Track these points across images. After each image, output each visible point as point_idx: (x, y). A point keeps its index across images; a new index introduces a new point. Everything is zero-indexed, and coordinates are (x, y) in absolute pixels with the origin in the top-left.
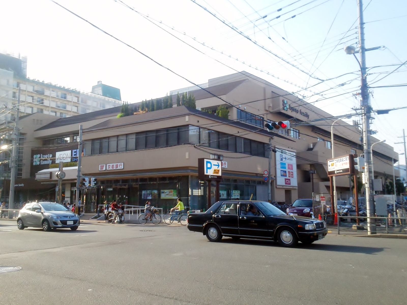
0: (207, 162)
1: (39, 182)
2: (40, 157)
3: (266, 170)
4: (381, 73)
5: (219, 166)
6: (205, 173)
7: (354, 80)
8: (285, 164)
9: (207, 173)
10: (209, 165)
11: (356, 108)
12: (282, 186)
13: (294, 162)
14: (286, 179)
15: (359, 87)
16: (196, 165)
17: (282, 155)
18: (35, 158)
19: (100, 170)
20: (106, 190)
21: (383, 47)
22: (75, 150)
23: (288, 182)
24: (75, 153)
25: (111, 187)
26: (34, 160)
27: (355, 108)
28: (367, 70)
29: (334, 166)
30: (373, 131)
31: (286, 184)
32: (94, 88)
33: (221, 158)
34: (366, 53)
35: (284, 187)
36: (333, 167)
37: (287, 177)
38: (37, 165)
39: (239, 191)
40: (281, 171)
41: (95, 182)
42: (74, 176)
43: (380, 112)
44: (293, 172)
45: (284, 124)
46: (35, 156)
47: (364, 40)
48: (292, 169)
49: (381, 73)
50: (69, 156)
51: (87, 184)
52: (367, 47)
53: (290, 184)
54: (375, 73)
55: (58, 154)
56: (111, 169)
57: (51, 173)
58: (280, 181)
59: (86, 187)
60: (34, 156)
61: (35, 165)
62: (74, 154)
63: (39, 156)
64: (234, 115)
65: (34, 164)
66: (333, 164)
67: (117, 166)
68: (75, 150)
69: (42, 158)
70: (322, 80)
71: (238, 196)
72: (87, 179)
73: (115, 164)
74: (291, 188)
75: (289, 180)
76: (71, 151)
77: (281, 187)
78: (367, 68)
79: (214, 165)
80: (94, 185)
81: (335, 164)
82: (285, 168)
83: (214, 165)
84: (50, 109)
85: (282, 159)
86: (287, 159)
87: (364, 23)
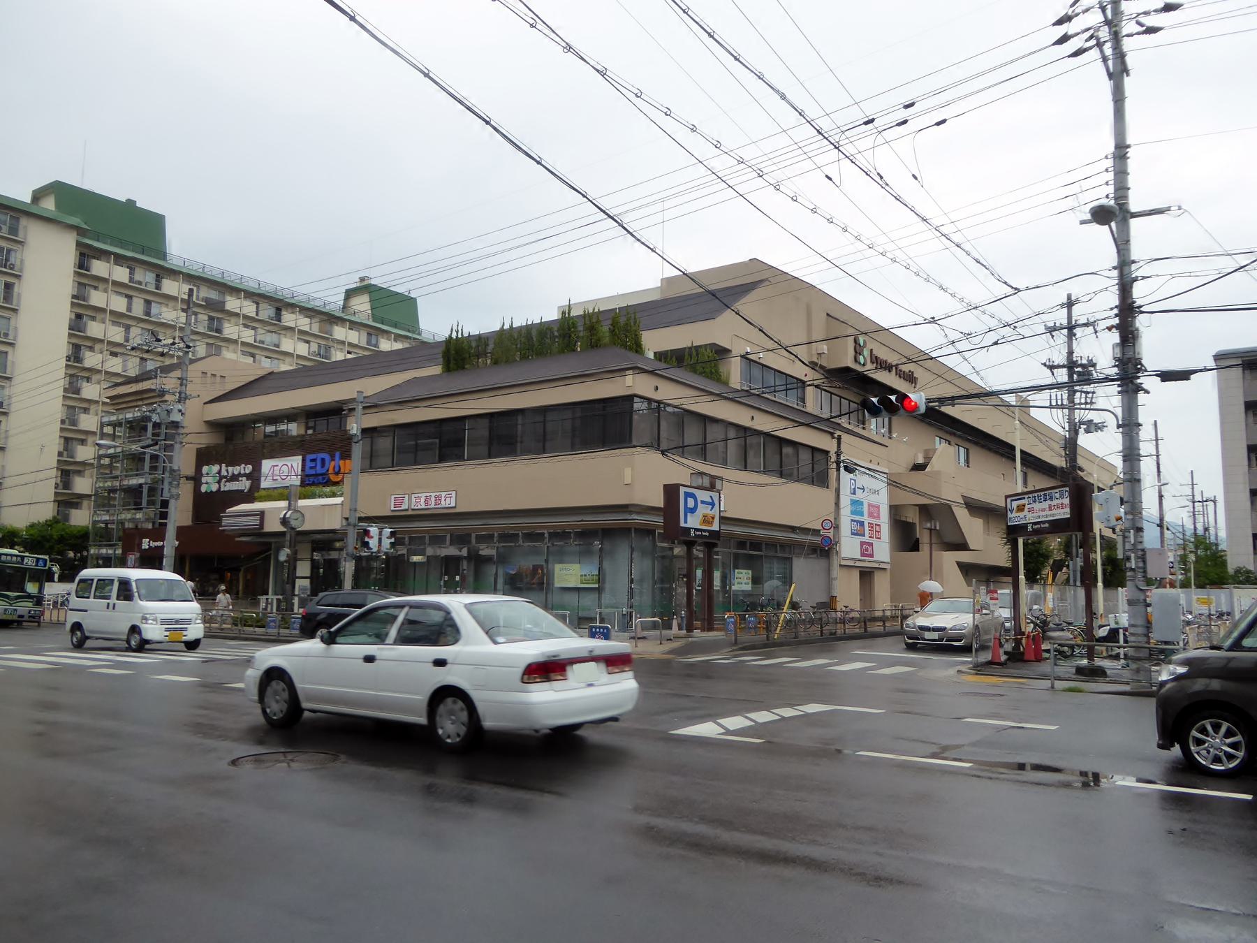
0: (687, 495)
1: (228, 537)
2: (219, 472)
3: (303, 512)
4: (1173, 276)
5: (713, 504)
6: (682, 524)
7: (1101, 291)
8: (861, 504)
9: (686, 522)
10: (691, 503)
11: (1053, 362)
12: (854, 562)
13: (882, 500)
14: (862, 543)
15: (1112, 309)
16: (659, 501)
17: (855, 481)
18: (208, 474)
19: (393, 508)
20: (408, 559)
21: (1177, 208)
22: (313, 456)
23: (866, 549)
24: (313, 464)
25: (422, 553)
26: (204, 480)
27: (1051, 364)
28: (1134, 267)
29: (1026, 512)
30: (1096, 424)
31: (863, 555)
32: (350, 294)
33: (718, 484)
34: (1134, 223)
35: (858, 564)
36: (1021, 514)
37: (866, 539)
38: (211, 492)
39: (750, 572)
40: (852, 520)
41: (393, 540)
42: (334, 523)
43: (1166, 376)
44: (879, 525)
45: (911, 401)
46: (205, 469)
47: (1129, 189)
48: (878, 517)
49: (1173, 276)
50: (296, 471)
51: (373, 543)
52: (1133, 208)
53: (872, 556)
54: (1157, 276)
55: (267, 465)
56: (423, 507)
57: (261, 514)
58: (849, 548)
59: (372, 550)
60: (202, 467)
61: (206, 492)
62: (309, 464)
63: (215, 468)
64: (735, 373)
65: (204, 489)
66: (1024, 506)
67: (438, 498)
68: (313, 456)
69: (224, 473)
70: (1016, 289)
71: (748, 583)
72: (374, 530)
73: (433, 495)
74: (876, 565)
75: (871, 545)
76: (300, 457)
77: (851, 563)
78: (1134, 262)
79: (703, 502)
80: (389, 547)
81: (1027, 507)
82: (862, 514)
83: (703, 502)
84: (347, 348)
85: (854, 489)
86: (866, 491)
87: (1129, 146)
